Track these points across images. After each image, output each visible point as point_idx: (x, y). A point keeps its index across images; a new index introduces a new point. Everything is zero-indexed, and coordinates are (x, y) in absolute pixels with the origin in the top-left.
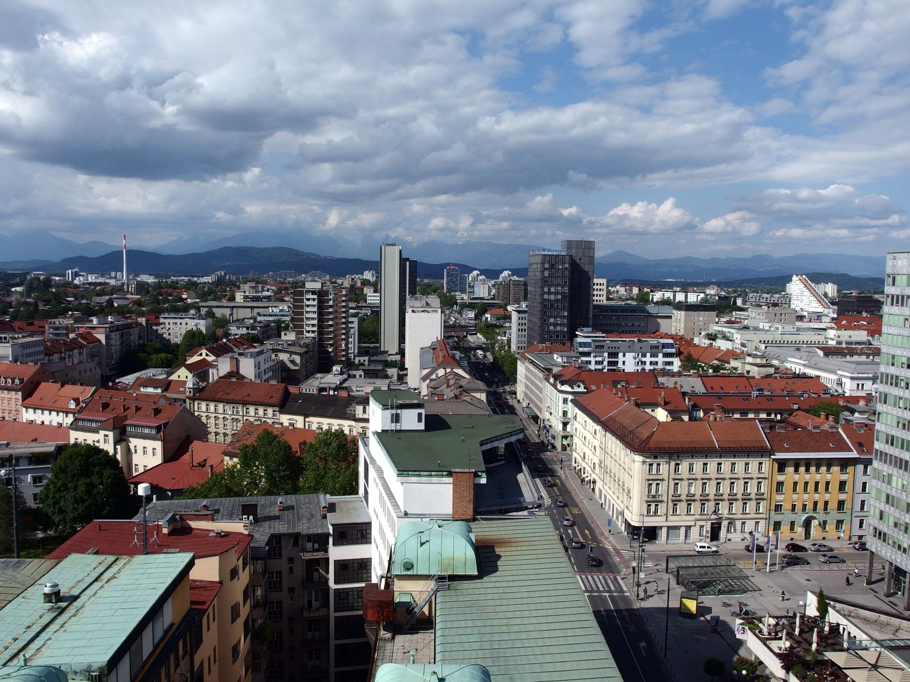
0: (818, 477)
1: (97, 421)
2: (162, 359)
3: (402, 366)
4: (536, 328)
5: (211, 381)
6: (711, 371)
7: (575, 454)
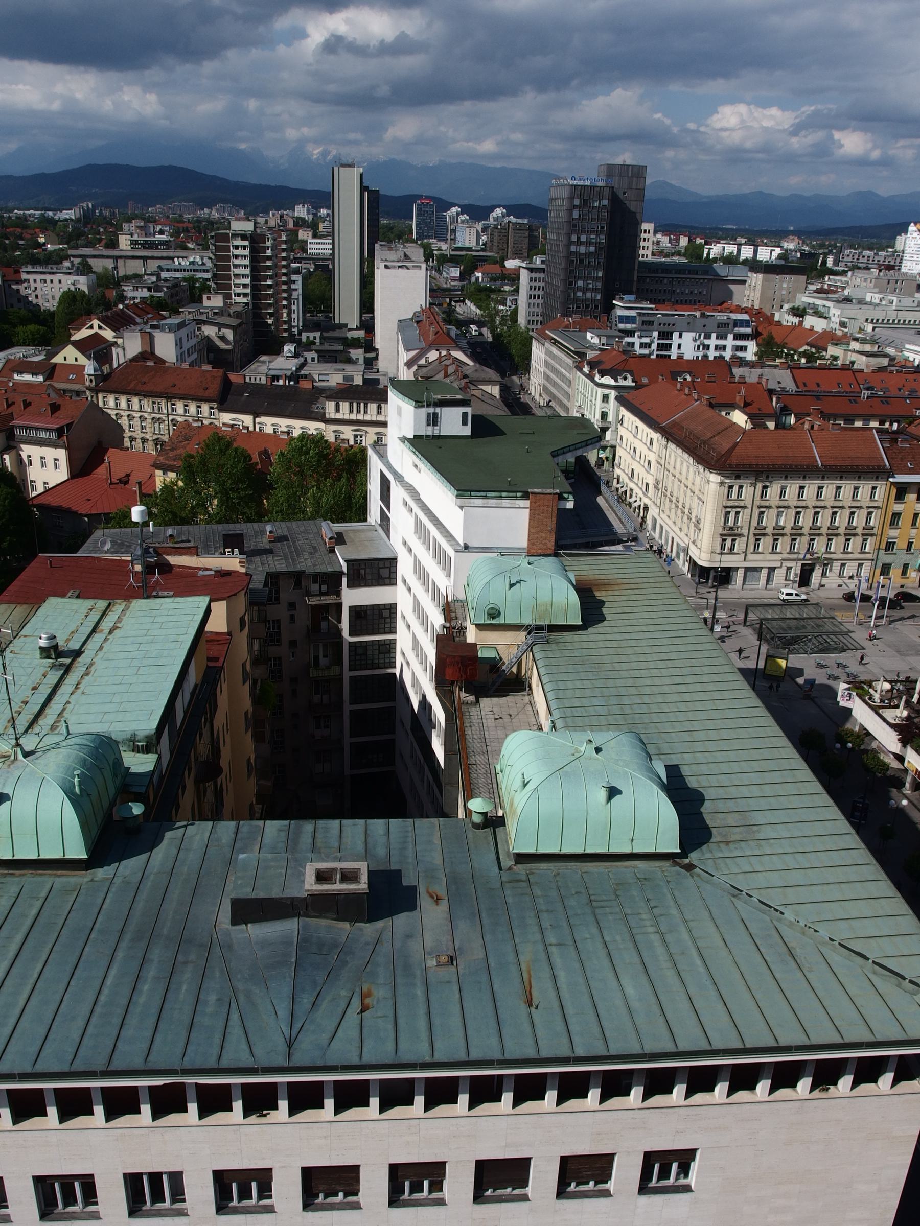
3: (369, 346)
4: (558, 294)
5: (115, 365)
6: (803, 360)
7: (617, 471)
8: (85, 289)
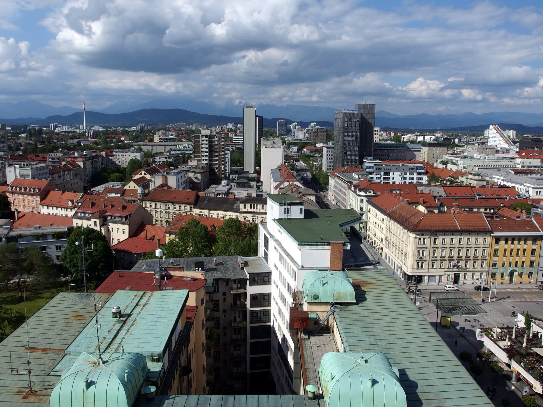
0: (519, 247)
1: (89, 213)
2: (116, 177)
3: (259, 181)
4: (340, 157)
5: (150, 189)
6: (448, 183)
8: (139, 158)
